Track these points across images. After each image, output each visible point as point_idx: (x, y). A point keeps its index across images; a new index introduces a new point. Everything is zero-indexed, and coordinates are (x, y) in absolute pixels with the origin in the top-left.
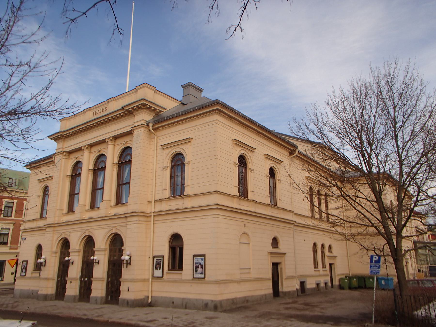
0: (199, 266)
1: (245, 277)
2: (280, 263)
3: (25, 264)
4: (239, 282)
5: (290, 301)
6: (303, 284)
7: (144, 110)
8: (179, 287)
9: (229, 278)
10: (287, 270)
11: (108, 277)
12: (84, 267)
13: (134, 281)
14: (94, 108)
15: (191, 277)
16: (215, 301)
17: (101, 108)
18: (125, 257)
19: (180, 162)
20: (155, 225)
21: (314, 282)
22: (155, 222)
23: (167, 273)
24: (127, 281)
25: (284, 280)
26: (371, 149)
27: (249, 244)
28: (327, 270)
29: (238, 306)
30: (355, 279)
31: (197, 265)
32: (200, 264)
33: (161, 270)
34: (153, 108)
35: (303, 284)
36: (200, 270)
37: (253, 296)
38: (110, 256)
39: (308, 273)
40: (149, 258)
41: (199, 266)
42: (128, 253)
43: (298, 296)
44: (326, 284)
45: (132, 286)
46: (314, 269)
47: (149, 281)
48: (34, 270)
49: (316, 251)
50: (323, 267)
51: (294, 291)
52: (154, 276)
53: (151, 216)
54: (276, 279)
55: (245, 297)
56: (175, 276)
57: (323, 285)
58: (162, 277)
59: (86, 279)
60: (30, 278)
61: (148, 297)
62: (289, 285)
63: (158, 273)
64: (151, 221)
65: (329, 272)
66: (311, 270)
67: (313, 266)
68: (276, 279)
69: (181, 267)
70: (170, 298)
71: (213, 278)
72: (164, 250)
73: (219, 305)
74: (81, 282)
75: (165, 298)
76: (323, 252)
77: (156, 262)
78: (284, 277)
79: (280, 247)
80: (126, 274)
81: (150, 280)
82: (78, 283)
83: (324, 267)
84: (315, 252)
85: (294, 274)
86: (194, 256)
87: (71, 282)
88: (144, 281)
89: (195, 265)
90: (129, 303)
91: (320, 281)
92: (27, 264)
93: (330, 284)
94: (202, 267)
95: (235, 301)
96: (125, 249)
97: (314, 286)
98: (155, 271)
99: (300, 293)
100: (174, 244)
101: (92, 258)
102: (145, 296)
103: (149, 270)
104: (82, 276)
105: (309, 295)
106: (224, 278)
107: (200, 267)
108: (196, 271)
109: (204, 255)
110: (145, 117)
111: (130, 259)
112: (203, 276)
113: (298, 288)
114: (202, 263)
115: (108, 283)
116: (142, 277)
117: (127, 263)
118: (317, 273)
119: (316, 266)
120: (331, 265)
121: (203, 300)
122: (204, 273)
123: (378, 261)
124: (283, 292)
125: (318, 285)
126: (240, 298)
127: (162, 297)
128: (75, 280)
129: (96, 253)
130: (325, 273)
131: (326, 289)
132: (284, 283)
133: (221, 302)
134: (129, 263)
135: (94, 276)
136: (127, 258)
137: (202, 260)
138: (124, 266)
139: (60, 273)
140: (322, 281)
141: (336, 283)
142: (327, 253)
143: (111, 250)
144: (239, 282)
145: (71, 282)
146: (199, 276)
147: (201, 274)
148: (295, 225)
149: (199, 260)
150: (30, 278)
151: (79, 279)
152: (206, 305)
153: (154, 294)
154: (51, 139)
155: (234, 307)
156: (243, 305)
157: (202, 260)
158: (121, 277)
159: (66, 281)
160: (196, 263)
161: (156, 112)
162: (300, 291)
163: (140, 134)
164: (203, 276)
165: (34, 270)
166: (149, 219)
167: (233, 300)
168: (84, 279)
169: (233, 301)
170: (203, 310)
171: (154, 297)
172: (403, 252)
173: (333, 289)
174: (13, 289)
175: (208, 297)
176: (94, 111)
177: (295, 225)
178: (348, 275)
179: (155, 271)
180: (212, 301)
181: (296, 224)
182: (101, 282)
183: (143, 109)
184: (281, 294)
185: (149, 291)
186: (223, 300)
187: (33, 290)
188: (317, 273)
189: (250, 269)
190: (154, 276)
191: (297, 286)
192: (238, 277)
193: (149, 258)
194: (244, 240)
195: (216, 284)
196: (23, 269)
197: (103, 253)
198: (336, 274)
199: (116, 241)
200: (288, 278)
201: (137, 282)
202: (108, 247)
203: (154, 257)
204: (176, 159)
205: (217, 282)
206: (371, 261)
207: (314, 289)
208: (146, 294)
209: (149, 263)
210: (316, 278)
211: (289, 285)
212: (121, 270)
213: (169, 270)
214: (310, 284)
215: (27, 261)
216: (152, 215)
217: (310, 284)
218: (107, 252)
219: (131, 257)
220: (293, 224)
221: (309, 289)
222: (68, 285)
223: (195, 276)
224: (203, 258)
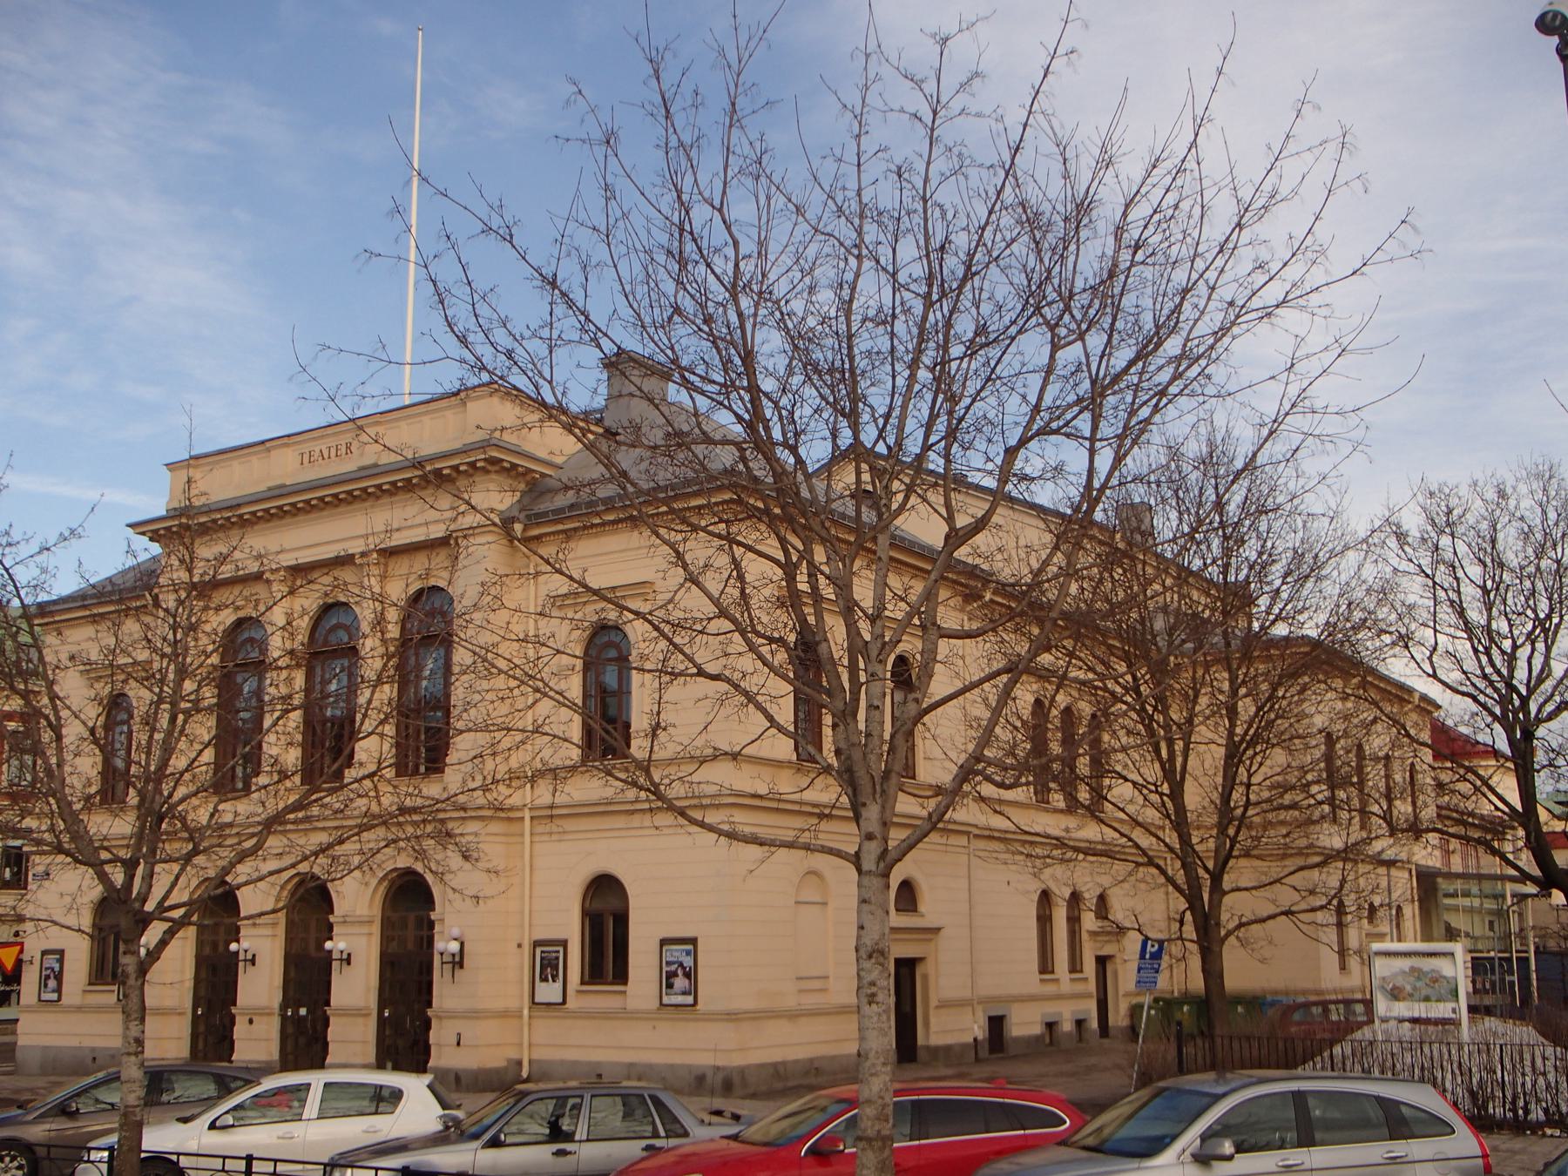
0: (680, 972)
1: (810, 1001)
2: (921, 959)
3: (51, 961)
4: (793, 1015)
5: (950, 1072)
6: (996, 1024)
7: (494, 476)
8: (621, 1033)
9: (763, 1004)
10: (944, 979)
11: (381, 1007)
12: (203, 975)
13: (474, 1015)
14: (304, 441)
15: (655, 1004)
16: (724, 1068)
17: (332, 442)
18: (445, 944)
19: (613, 653)
20: (537, 846)
21: (1039, 1018)
22: (536, 838)
23: (579, 992)
24: (453, 1015)
25: (932, 1012)
26: (1170, 643)
27: (825, 904)
28: (1086, 979)
29: (790, 1084)
30: (1185, 1008)
31: (673, 968)
32: (681, 965)
33: (559, 985)
34: (506, 465)
35: (996, 1024)
36: (680, 982)
37: (834, 1057)
38: (386, 939)
39: (1015, 990)
40: (519, 946)
41: (680, 972)
42: (456, 932)
43: (977, 1060)
44: (1080, 1023)
45: (470, 1030)
46: (1038, 977)
47: (521, 1017)
48: (90, 984)
49: (1050, 918)
50: (1073, 970)
51: (964, 1046)
52: (537, 1000)
53: (522, 819)
54: (907, 1009)
55: (811, 1060)
56: (602, 999)
57: (1067, 1026)
58: (564, 1002)
59: (303, 1011)
60: (79, 1009)
61: (520, 1063)
62: (949, 1026)
63: (549, 992)
64: (522, 835)
65: (1092, 986)
66: (1026, 976)
67: (1035, 966)
68: (907, 1009)
69: (621, 976)
70: (589, 1063)
71: (720, 1006)
72: (569, 926)
73: (736, 1080)
74: (284, 1017)
75: (575, 1063)
76: (1074, 921)
77: (542, 959)
78: (933, 1002)
79: (922, 908)
80: (446, 994)
81: (526, 1012)
82: (276, 1022)
83: (1075, 966)
84: (1044, 920)
85: (967, 993)
86: (664, 942)
87: (251, 1022)
88: (504, 1014)
89: (1329, 1073)
90: (464, 1081)
91: (1060, 1014)
92: (61, 961)
93: (1094, 1024)
94: (687, 975)
95: (782, 1070)
96: (442, 920)
97: (1037, 1030)
98: (540, 986)
99: (984, 1052)
100: (598, 905)
101: (328, 945)
102: (509, 1061)
103: (522, 982)
104: (284, 1006)
105: (1015, 1057)
106: (749, 1004)
107: (681, 970)
108: (670, 986)
109: (693, 941)
110: (494, 497)
111: (462, 944)
112: (689, 999)
113: (980, 1037)
114: (57, 967)
115: (382, 1022)
116: (498, 1005)
117: (453, 963)
118: (1050, 989)
119: (1046, 966)
120: (1102, 961)
121: (689, 1068)
122: (693, 991)
123: (1157, 956)
124: (928, 1048)
125: (1050, 1026)
126: (796, 1062)
127: (562, 1062)
128: (265, 1012)
129: (336, 930)
130: (1079, 988)
131: (1080, 1040)
132: (933, 1020)
133: (742, 1071)
134: (458, 962)
135: (335, 1000)
136: (454, 947)
137: (688, 953)
138: (335, 965)
139: (202, 993)
140: (1066, 1016)
141: (1119, 1017)
142: (1089, 921)
143: (386, 924)
144: (793, 1015)
145: (251, 1022)
146: (680, 999)
147: (684, 993)
148: (976, 836)
149: (677, 953)
150: (79, 1009)
151: (277, 1011)
152: (700, 1079)
153: (540, 1054)
154: (143, 534)
155: (779, 1085)
156: (805, 1082)
157: (688, 953)
158: (430, 1004)
159: (233, 1018)
160: (668, 963)
161: (528, 478)
162: (987, 1045)
163: (485, 556)
164: (689, 999)
165: (90, 984)
166: (514, 828)
167: (775, 1065)
168: (296, 1012)
169: (777, 1071)
170: (691, 1094)
171: (538, 1061)
172: (1223, 933)
173: (1105, 1041)
174: (12, 1047)
175: (704, 1060)
176: (306, 448)
177: (976, 836)
178: (1168, 996)
179: (540, 986)
180: (718, 1068)
181: (977, 832)
182: (360, 1020)
183: (488, 472)
184: (921, 1054)
185: (521, 1045)
186: (749, 1067)
187: (93, 1049)
188: (1050, 989)
189: (827, 977)
190: (537, 1000)
191: (979, 1030)
192: (791, 1002)
193: (519, 946)
194: (810, 894)
195: (728, 1020)
196: (48, 977)
197: (365, 930)
198: (1121, 993)
199: (409, 898)
200: (944, 1005)
201: (486, 1018)
202: (377, 911)
203: (536, 944)
204: (598, 641)
205: (732, 1017)
206: (1142, 956)
207: (1038, 1039)
208: (513, 1054)
209: (519, 964)
210: (1045, 1002)
211: (949, 1026)
212: (430, 984)
213: (583, 983)
214: (1024, 1024)
215: (61, 952)
216: (527, 815)
217: (1024, 1024)
218: (376, 929)
219: (462, 944)
220: (968, 833)
221: (1017, 1040)
222: (240, 1030)
223: (666, 1000)
224: (690, 947)
